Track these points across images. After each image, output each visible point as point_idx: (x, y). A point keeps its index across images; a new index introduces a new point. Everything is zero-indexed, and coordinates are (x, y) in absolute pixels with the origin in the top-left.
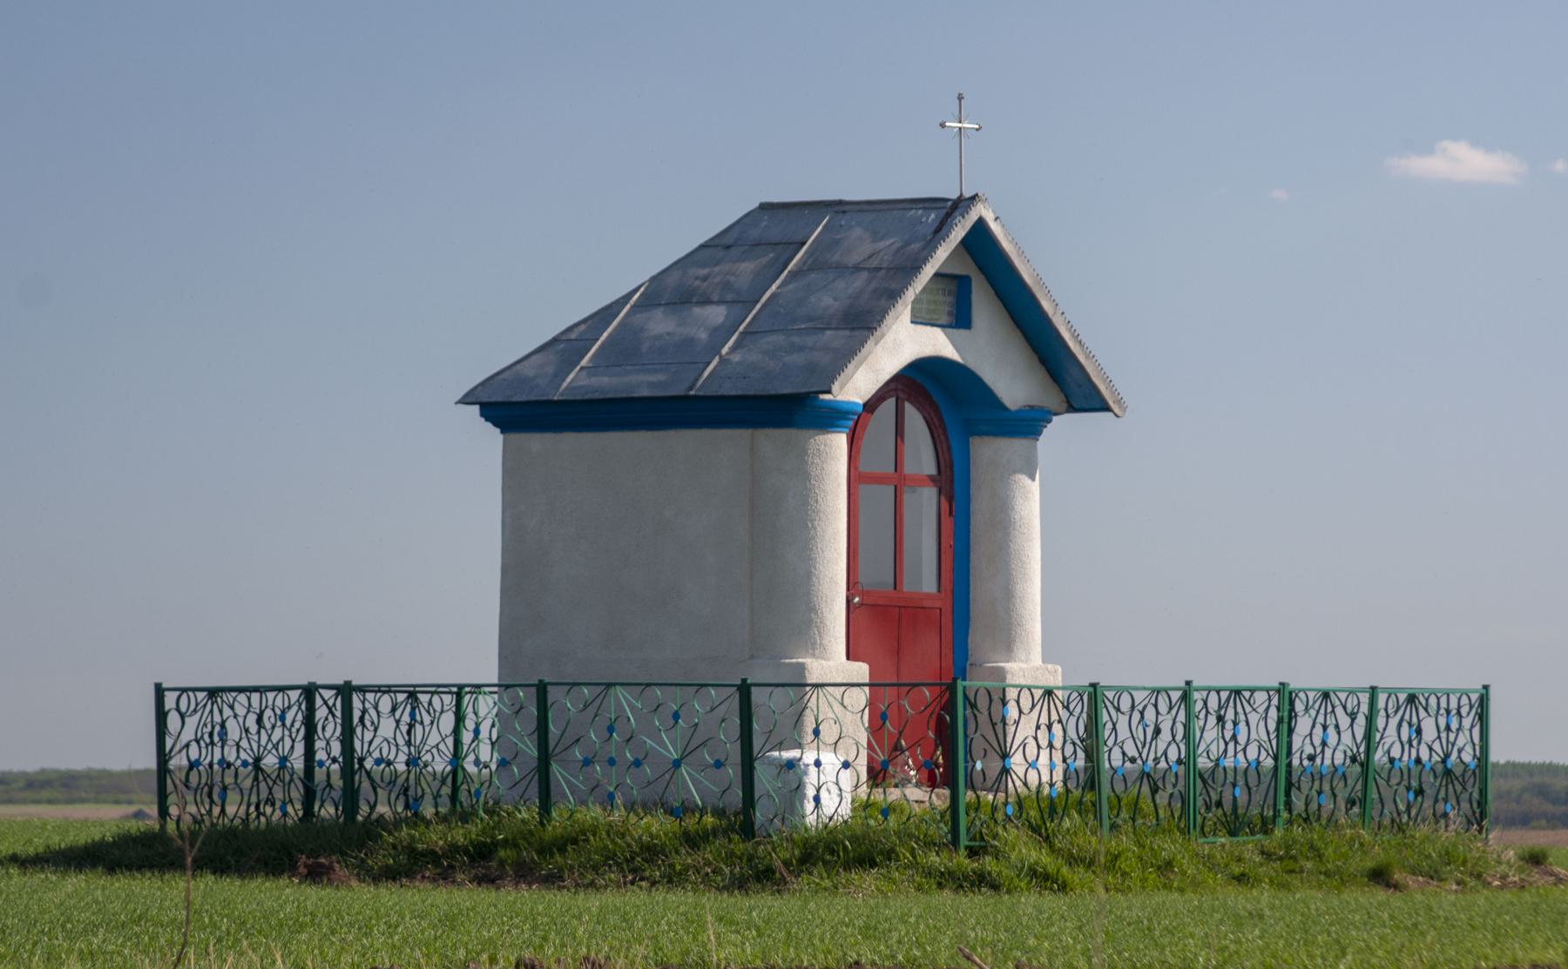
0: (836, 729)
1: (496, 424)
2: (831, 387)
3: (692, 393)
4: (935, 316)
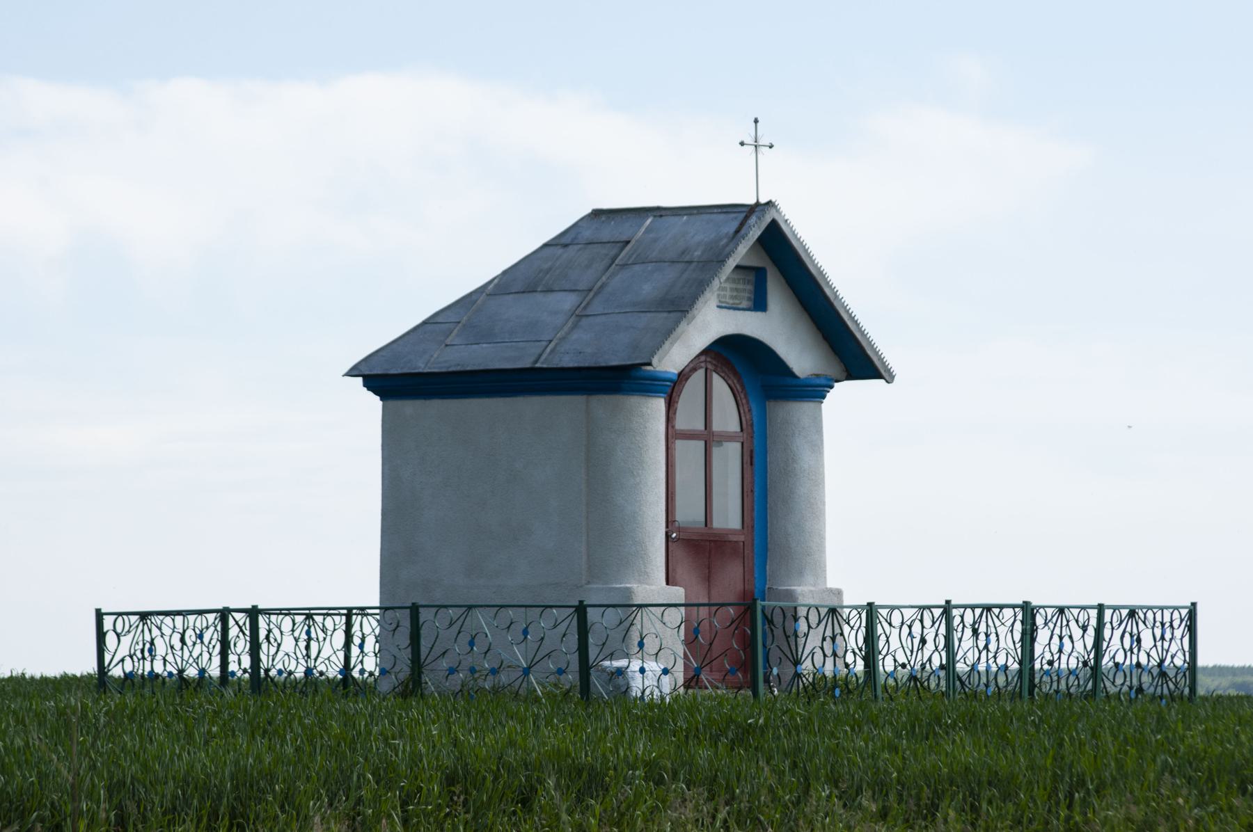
0: (657, 641)
1: (376, 393)
2: (651, 360)
3: (538, 365)
4: (737, 301)
